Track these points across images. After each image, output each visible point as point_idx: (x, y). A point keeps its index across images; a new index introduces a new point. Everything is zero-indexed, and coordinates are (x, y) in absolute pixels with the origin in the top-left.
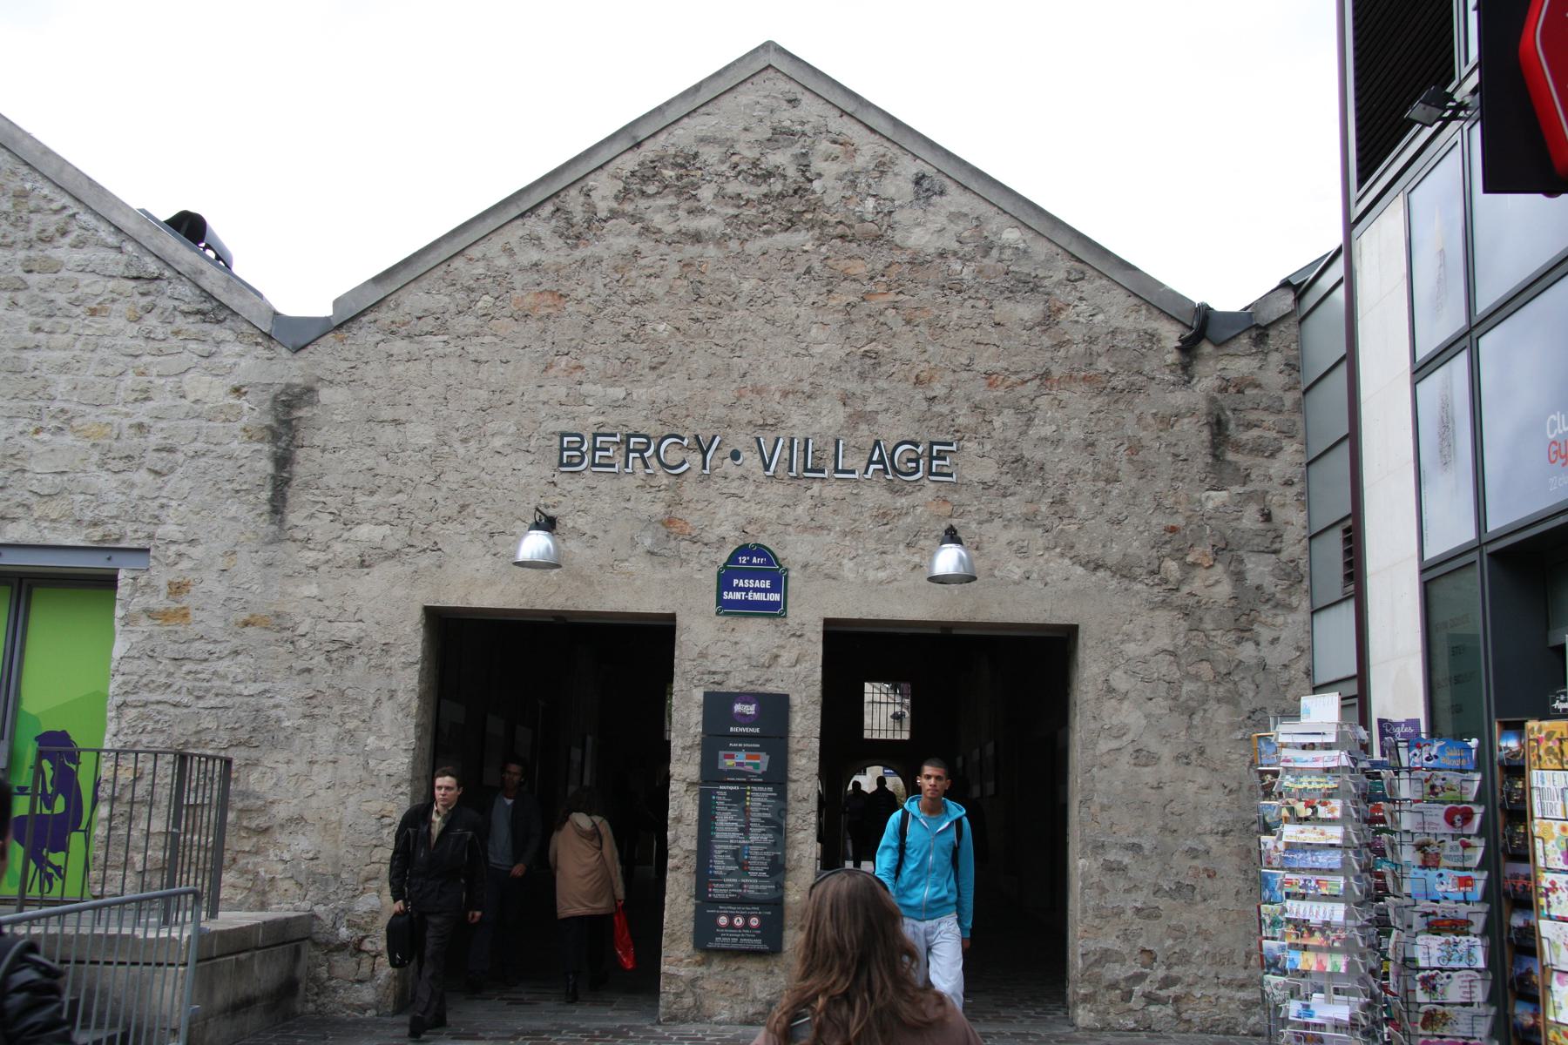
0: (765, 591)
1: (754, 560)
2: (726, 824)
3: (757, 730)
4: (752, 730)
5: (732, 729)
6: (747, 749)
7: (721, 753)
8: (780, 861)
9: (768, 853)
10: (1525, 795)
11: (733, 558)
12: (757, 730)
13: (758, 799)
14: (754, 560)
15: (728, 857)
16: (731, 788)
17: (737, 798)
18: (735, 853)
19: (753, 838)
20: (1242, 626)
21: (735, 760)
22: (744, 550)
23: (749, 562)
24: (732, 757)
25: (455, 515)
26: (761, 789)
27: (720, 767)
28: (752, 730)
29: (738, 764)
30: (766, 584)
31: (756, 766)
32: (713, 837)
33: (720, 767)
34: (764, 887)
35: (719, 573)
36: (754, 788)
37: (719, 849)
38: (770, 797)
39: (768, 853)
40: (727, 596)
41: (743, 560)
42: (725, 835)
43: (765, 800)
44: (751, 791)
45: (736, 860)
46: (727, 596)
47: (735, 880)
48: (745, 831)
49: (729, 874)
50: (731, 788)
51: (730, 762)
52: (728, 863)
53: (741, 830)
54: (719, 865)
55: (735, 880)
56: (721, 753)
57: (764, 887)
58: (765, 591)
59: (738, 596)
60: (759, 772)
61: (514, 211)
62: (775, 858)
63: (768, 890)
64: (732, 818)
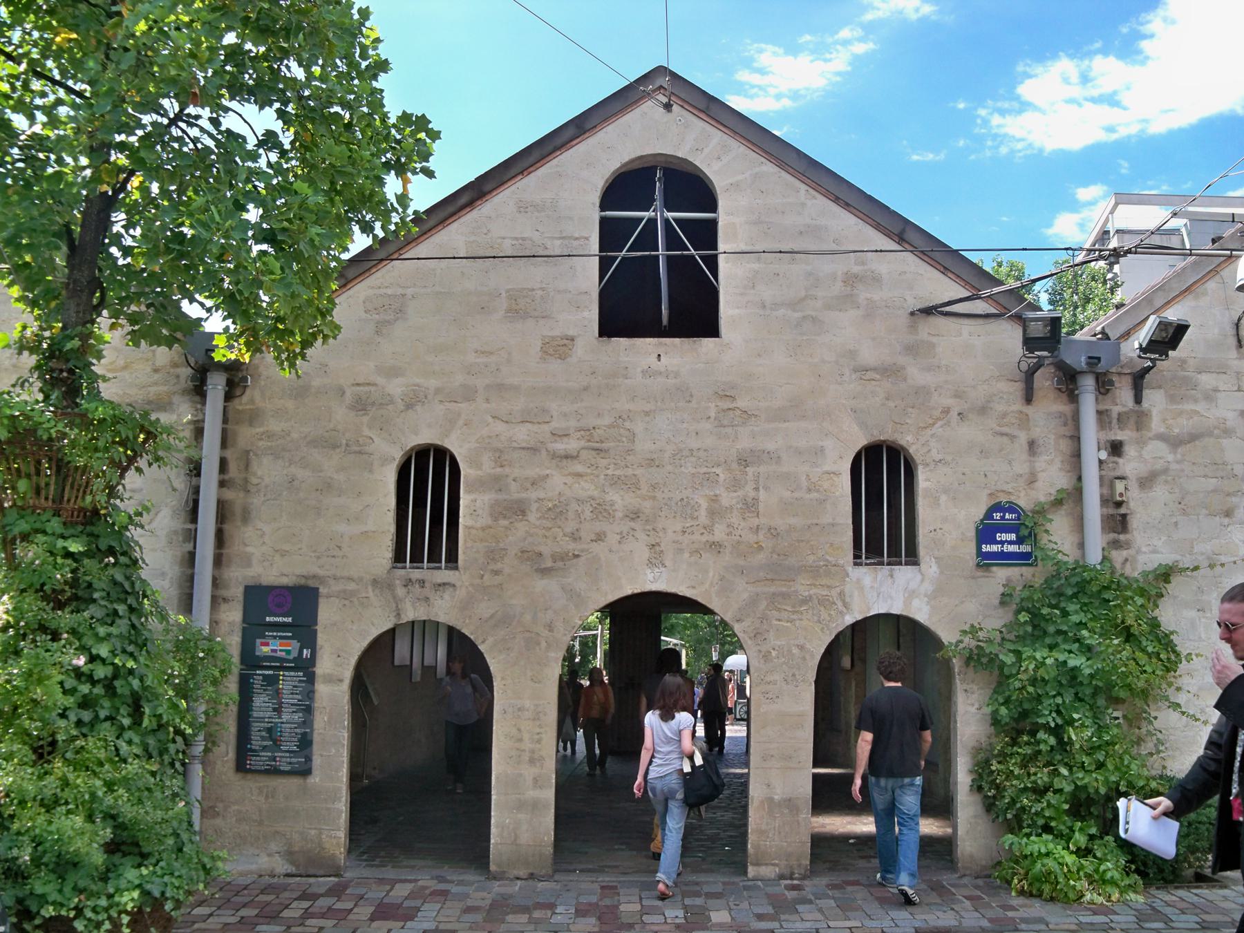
0: (1011, 543)
1: (1007, 516)
2: (261, 702)
3: (290, 620)
4: (285, 620)
5: (268, 619)
6: (281, 638)
7: (258, 641)
8: (309, 738)
9: (298, 731)
10: (313, 692)
11: (989, 515)
12: (290, 620)
13: (288, 682)
14: (1007, 516)
15: (264, 734)
16: (267, 672)
17: (271, 681)
18: (269, 730)
19: (285, 717)
20: (33, 470)
21: (268, 648)
22: (997, 507)
23: (1003, 518)
24: (267, 644)
25: (544, 453)
26: (292, 674)
27: (257, 654)
28: (285, 620)
29: (273, 651)
30: (1013, 537)
31: (288, 652)
32: (250, 716)
33: (257, 654)
34: (294, 760)
35: (977, 527)
36: (286, 673)
37: (255, 727)
38: (300, 681)
39: (298, 731)
40: (986, 548)
41: (997, 516)
42: (261, 715)
43: (296, 684)
44: (283, 675)
45: (270, 736)
46: (986, 548)
47: (269, 754)
48: (278, 710)
49: (265, 748)
50: (267, 672)
51: (265, 649)
52: (263, 738)
53: (275, 710)
54: (256, 742)
55: (269, 754)
56: (258, 641)
57: (294, 760)
58: (1011, 543)
59: (995, 548)
60: (291, 657)
61: (559, 141)
62: (304, 735)
63: (298, 763)
64: (266, 699)
